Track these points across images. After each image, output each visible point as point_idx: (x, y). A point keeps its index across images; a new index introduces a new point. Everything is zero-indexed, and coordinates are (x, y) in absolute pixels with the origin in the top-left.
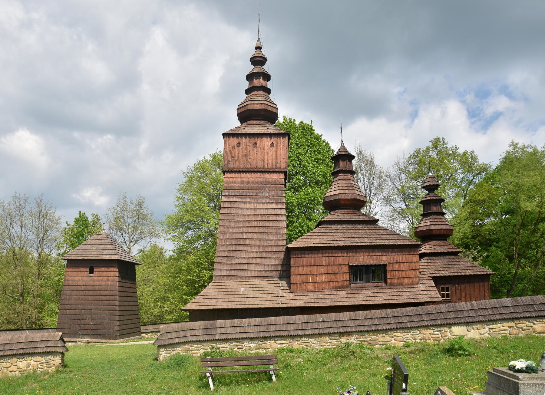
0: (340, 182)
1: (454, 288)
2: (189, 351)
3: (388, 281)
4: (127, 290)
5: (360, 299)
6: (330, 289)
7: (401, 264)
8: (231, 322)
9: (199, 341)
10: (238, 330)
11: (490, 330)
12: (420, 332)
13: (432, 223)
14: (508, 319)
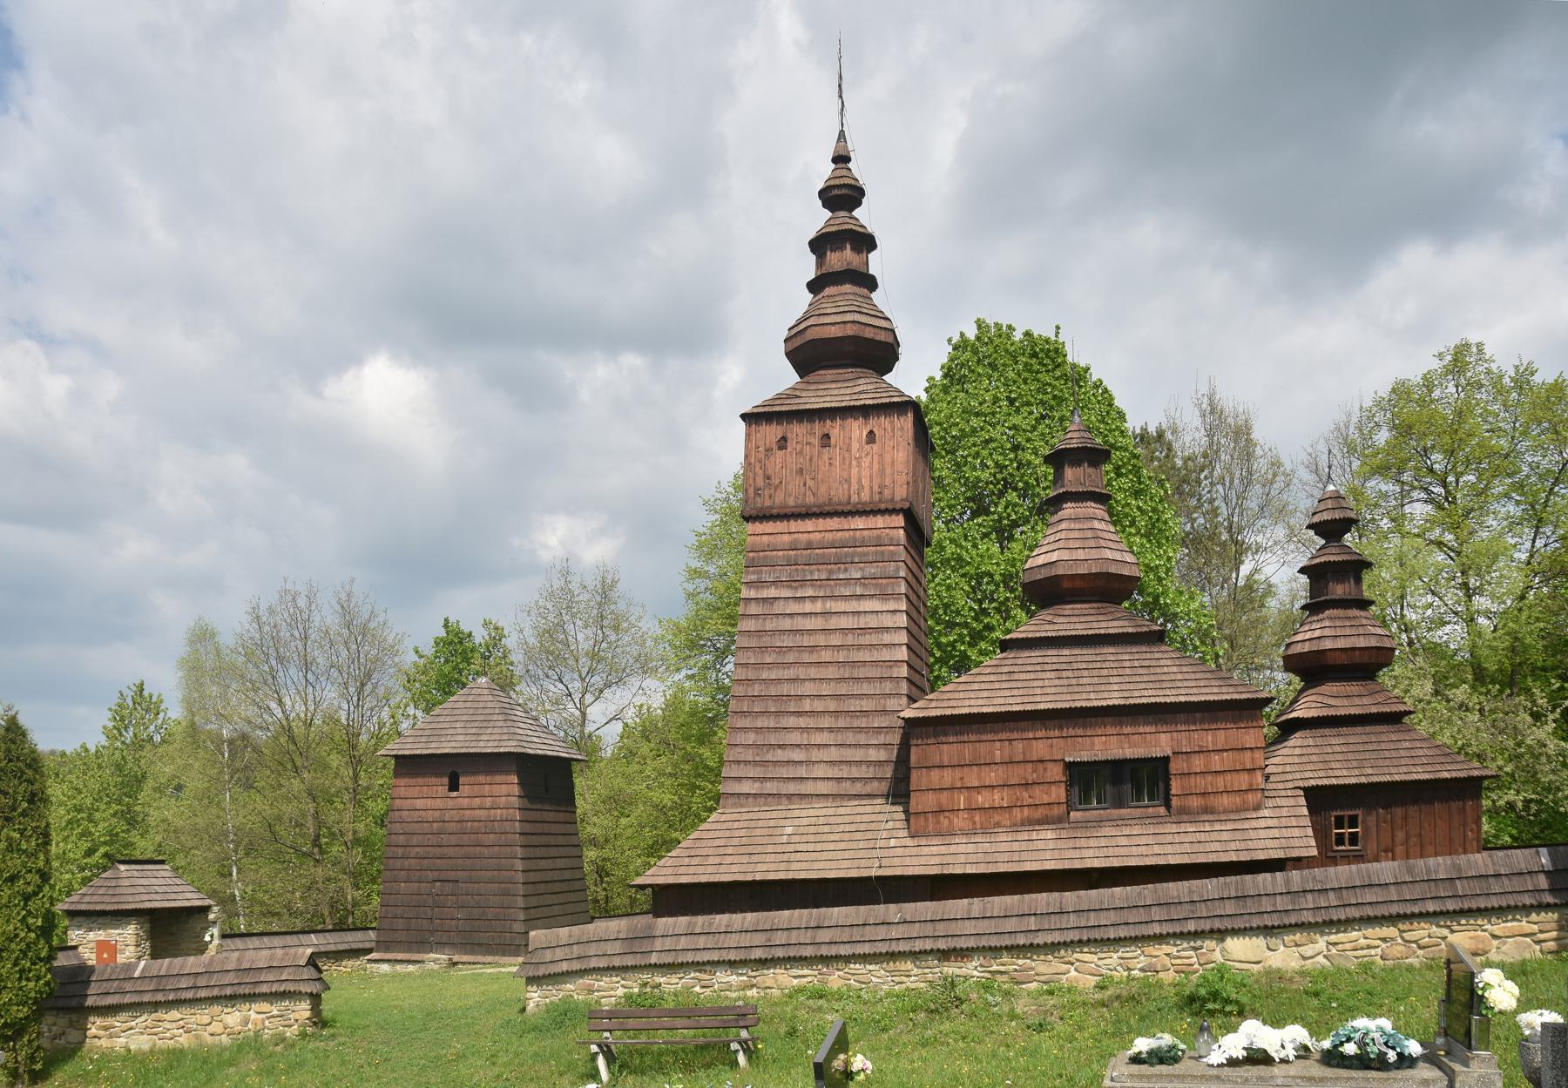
0: (1064, 525)
1: (1372, 820)
2: (593, 991)
3: (1175, 802)
4: (546, 828)
5: (1090, 853)
6: (1015, 825)
7: (1212, 754)
8: (690, 923)
9: (614, 967)
10: (702, 942)
11: (1330, 947)
12: (1143, 952)
13: (1327, 632)
14: (1376, 918)
